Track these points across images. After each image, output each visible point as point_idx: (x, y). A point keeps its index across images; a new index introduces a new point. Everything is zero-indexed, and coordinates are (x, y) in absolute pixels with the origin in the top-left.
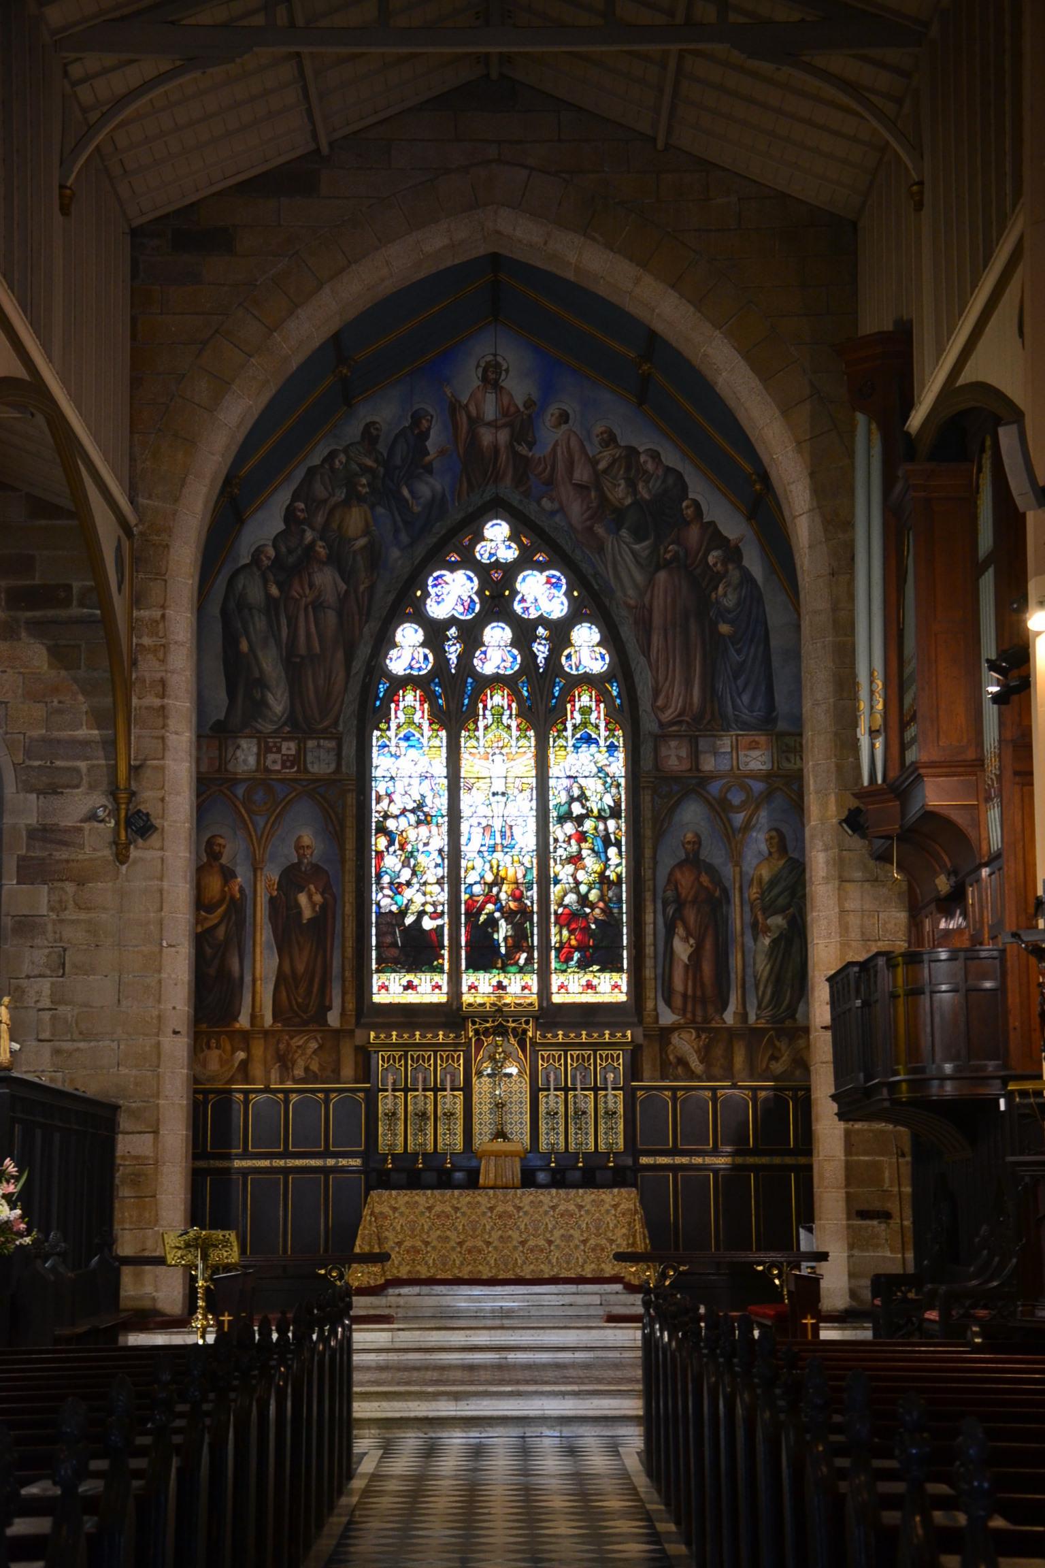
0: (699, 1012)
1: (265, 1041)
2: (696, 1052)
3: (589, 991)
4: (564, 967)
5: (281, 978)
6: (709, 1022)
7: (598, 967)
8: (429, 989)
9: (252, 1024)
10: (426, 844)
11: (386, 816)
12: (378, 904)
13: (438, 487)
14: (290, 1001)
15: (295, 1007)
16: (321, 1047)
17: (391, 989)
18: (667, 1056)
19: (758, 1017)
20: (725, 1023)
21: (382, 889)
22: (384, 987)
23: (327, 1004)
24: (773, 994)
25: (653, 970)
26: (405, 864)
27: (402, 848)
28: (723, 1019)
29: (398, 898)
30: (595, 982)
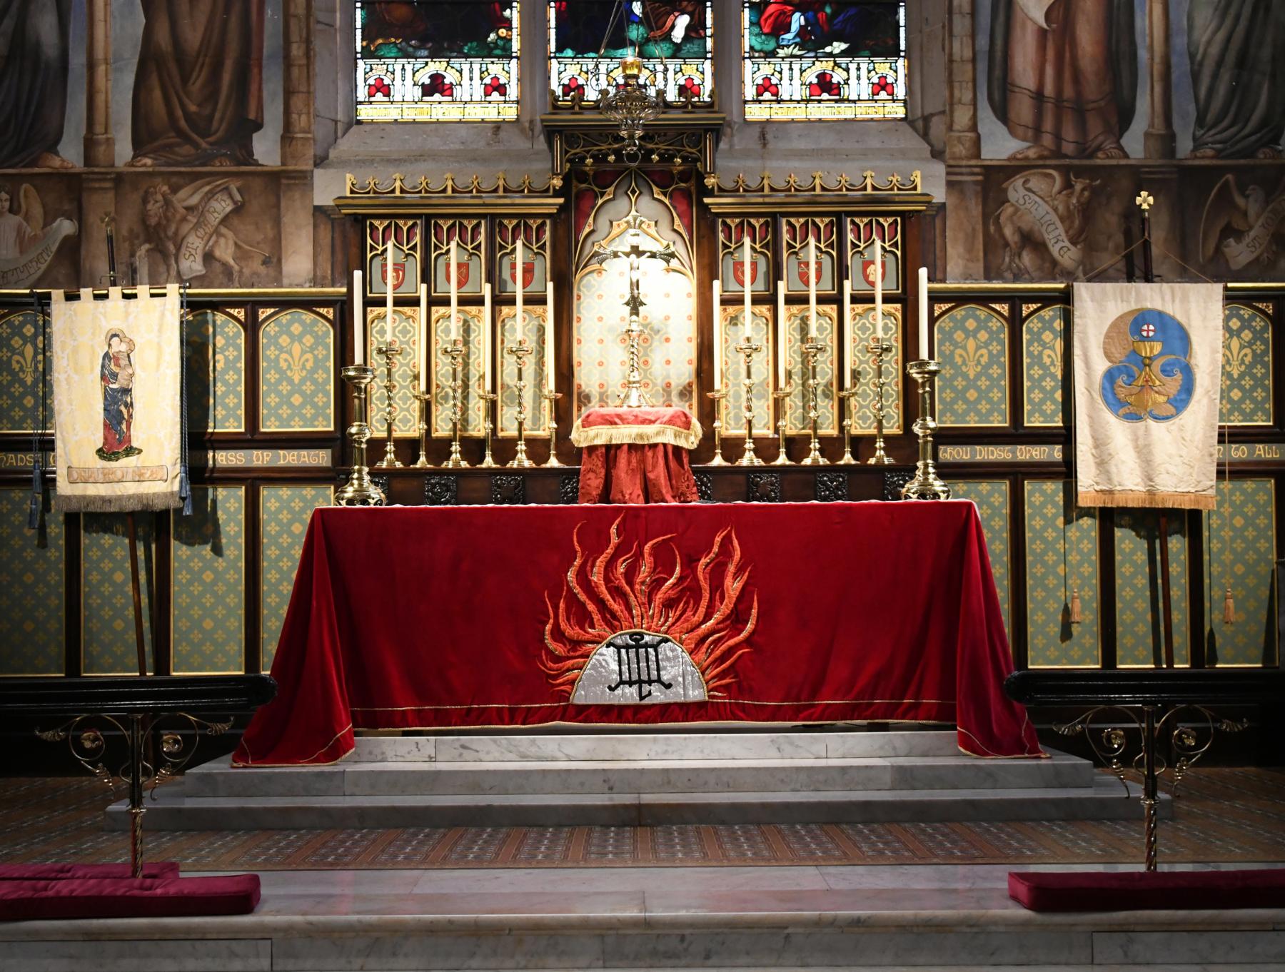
0: (1069, 133)
1: (117, 195)
2: (1062, 219)
3: (825, 96)
4: (771, 45)
5: (149, 60)
6: (1092, 156)
7: (844, 46)
8: (479, 92)
9: (89, 159)
14: (170, 113)
15: (183, 123)
16: (238, 210)
17: (397, 93)
18: (999, 229)
19: (1198, 144)
20: (1126, 156)
22: (382, 88)
23: (252, 116)
24: (1232, 92)
25: (967, 41)
28: (1121, 148)
30: (838, 77)
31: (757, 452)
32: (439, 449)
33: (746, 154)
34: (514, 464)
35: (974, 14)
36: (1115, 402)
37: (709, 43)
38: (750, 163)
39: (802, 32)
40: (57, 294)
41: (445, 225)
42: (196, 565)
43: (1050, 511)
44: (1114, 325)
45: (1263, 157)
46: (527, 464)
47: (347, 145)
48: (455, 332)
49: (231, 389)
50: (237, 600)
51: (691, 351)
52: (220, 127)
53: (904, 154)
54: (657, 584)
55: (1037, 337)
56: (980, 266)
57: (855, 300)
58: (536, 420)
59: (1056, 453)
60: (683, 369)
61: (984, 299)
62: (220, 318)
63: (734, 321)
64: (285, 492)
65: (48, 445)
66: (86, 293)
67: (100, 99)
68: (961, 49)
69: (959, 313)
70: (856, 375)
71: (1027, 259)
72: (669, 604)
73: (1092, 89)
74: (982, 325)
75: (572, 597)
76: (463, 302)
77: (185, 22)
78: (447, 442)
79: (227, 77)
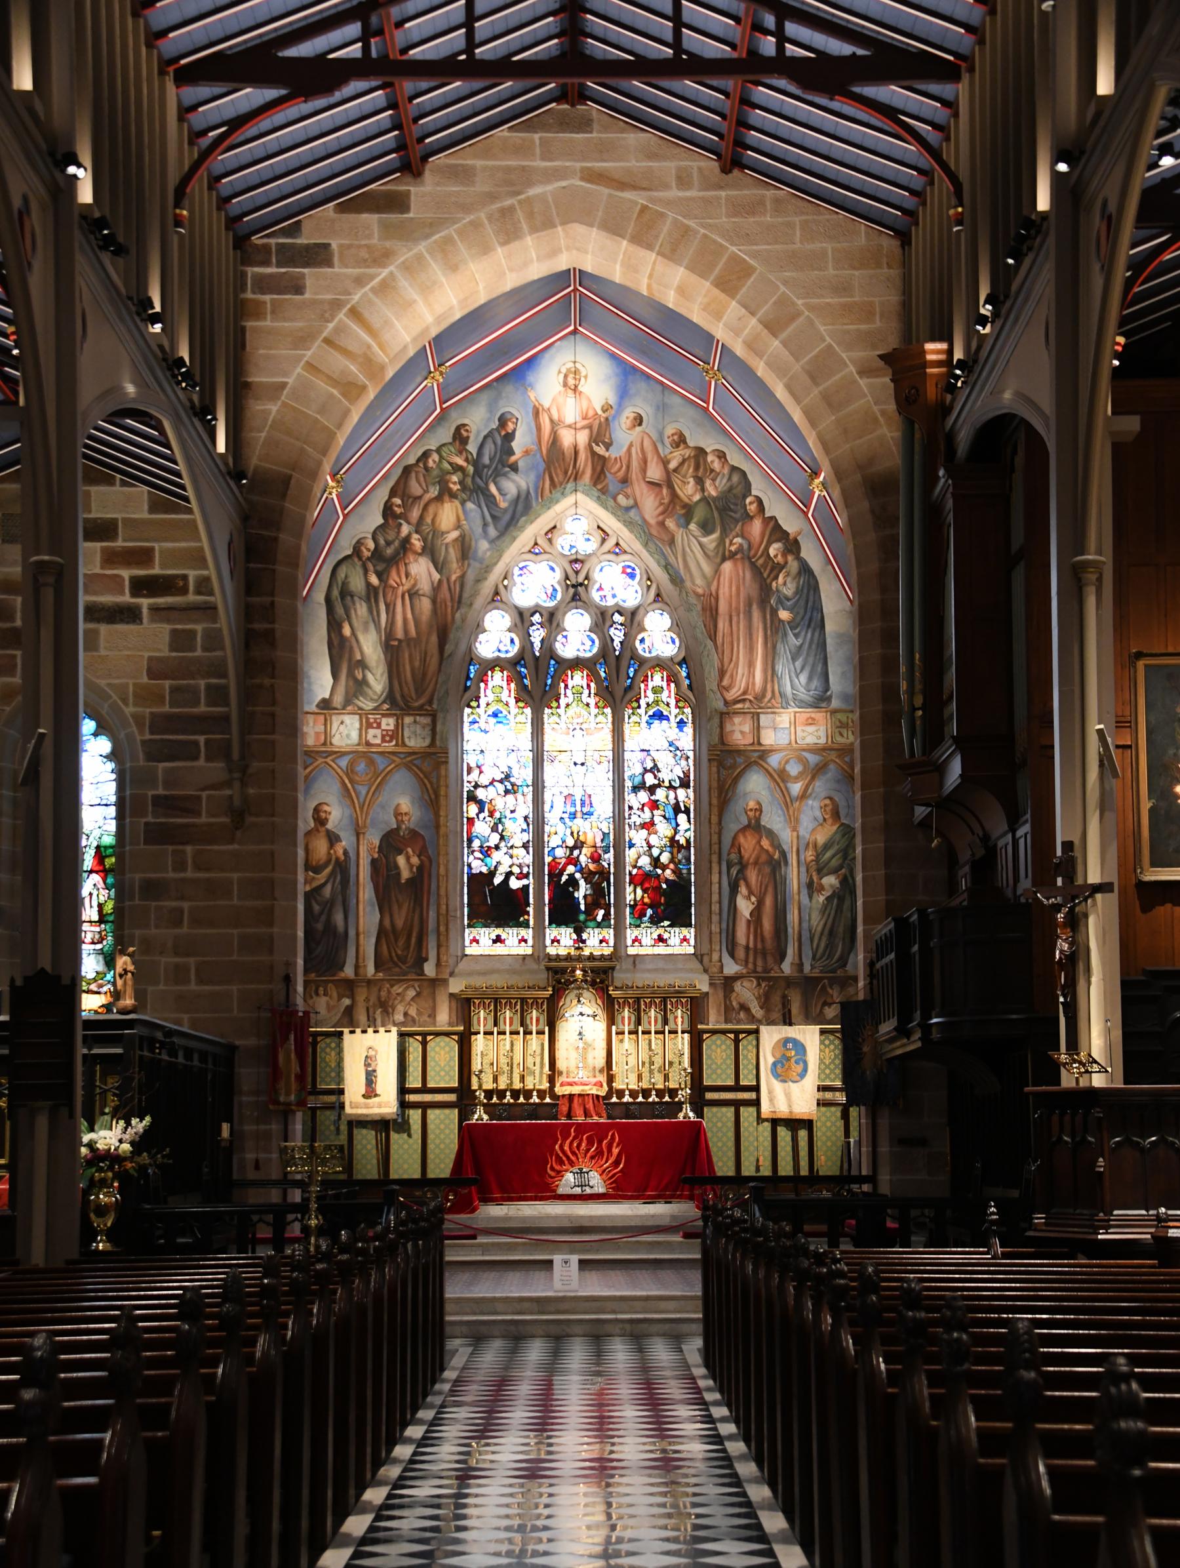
0: (760, 963)
4: (638, 922)
5: (381, 933)
9: (356, 974)
10: (512, 812)
11: (476, 786)
12: (469, 866)
13: (523, 485)
16: (418, 994)
19: (813, 967)
21: (473, 852)
24: (827, 946)
26: (494, 829)
27: (491, 815)
29: (488, 860)
30: (666, 936)
31: (630, 1096)
32: (501, 1094)
33: (627, 971)
34: (532, 1101)
35: (720, 914)
36: (777, 1075)
37: (612, 922)
38: (629, 975)
39: (651, 916)
40: (346, 1031)
41: (503, 1001)
42: (401, 1142)
43: (751, 1119)
44: (779, 1041)
45: (839, 973)
46: (537, 1101)
47: (462, 966)
48: (508, 1047)
49: (416, 1069)
50: (417, 1156)
51: (604, 1053)
52: (410, 960)
53: (691, 971)
54: (588, 1151)
55: (745, 1047)
56: (723, 1019)
57: (670, 1032)
58: (541, 1082)
59: (753, 1095)
60: (601, 1061)
61: (724, 1032)
62: (411, 1040)
63: (622, 1041)
64: (437, 1111)
65: (341, 1092)
66: (358, 1031)
67: (361, 949)
68: (715, 928)
69: (714, 1037)
70: (671, 1063)
71: (742, 1015)
72: (592, 1158)
73: (769, 943)
74: (723, 1043)
75: (557, 1155)
76: (511, 1033)
77: (396, 916)
78: (505, 1091)
79: (413, 940)
